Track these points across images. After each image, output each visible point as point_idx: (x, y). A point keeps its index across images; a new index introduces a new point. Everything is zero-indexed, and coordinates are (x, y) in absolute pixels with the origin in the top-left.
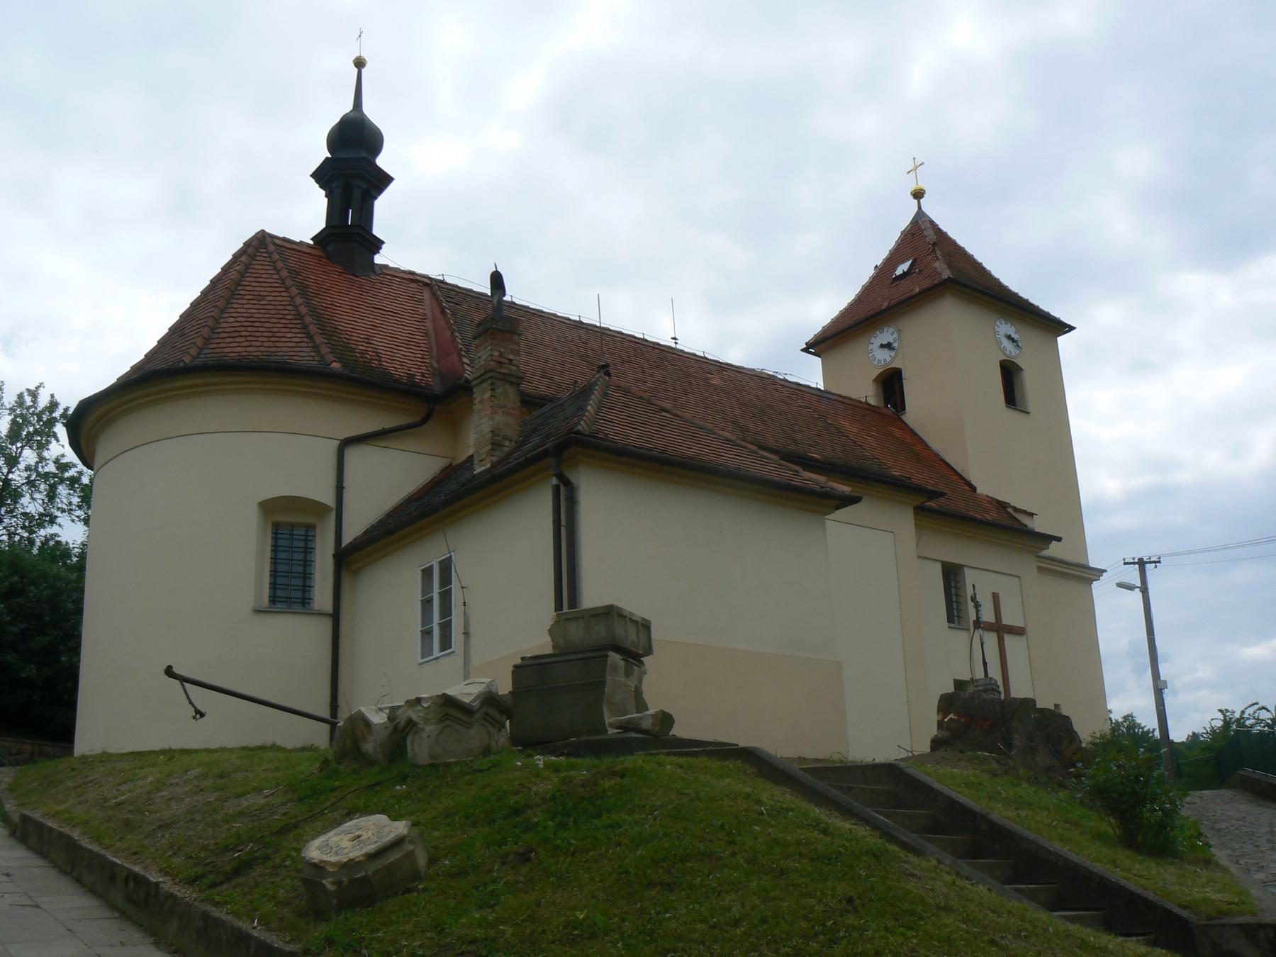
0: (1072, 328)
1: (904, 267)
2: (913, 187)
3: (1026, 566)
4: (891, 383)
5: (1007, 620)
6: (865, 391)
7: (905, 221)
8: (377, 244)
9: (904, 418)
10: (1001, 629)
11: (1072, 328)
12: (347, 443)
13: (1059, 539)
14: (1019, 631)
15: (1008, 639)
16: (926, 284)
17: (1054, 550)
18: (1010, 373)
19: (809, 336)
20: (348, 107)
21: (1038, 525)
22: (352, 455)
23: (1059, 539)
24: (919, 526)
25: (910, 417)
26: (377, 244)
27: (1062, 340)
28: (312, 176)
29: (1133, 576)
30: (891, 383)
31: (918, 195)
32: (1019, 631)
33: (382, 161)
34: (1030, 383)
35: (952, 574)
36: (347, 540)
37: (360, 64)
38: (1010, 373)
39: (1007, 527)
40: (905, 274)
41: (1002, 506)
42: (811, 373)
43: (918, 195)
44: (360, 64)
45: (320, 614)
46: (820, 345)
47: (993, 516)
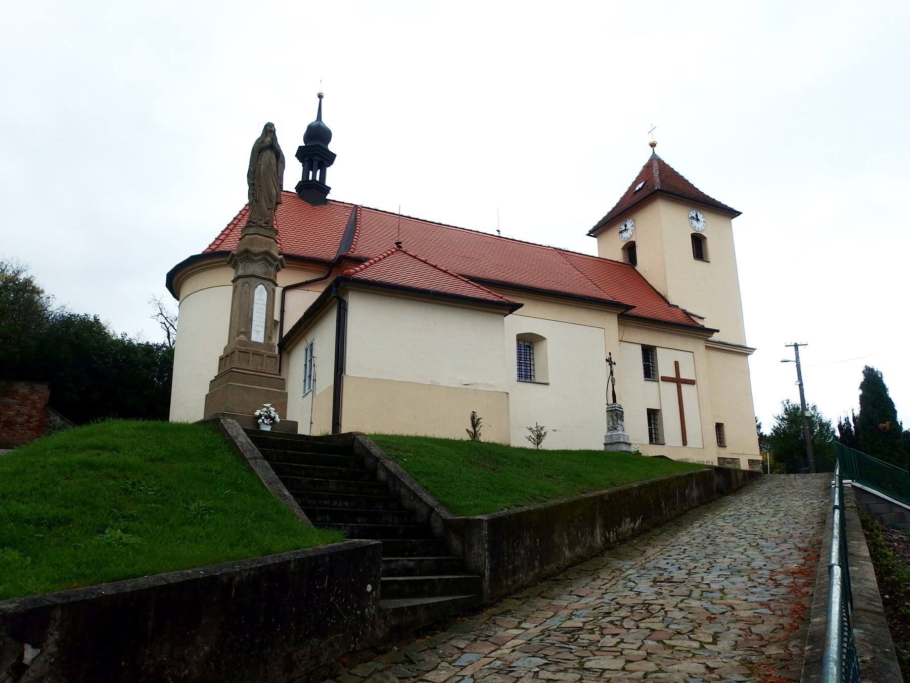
0: (740, 213)
1: (640, 186)
2: (651, 141)
3: (698, 346)
4: (630, 249)
5: (683, 376)
6: (617, 255)
7: (645, 161)
8: (327, 190)
9: (636, 268)
10: (678, 381)
11: (740, 213)
12: (286, 289)
13: (718, 331)
14: (692, 382)
15: (684, 387)
16: (647, 193)
17: (715, 337)
18: (698, 242)
19: (591, 227)
20: (313, 118)
21: (707, 324)
22: (290, 295)
23: (718, 331)
24: (620, 324)
25: (639, 268)
26: (327, 190)
27: (735, 221)
28: (335, 156)
29: (790, 354)
30: (630, 249)
31: (653, 145)
32: (692, 382)
33: (331, 147)
34: (712, 247)
35: (648, 353)
36: (285, 333)
37: (320, 96)
38: (698, 242)
39: (689, 327)
40: (640, 189)
41: (688, 315)
42: (591, 247)
43: (653, 145)
44: (320, 96)
45: (665, 379)
46: (597, 231)
47: (682, 319)
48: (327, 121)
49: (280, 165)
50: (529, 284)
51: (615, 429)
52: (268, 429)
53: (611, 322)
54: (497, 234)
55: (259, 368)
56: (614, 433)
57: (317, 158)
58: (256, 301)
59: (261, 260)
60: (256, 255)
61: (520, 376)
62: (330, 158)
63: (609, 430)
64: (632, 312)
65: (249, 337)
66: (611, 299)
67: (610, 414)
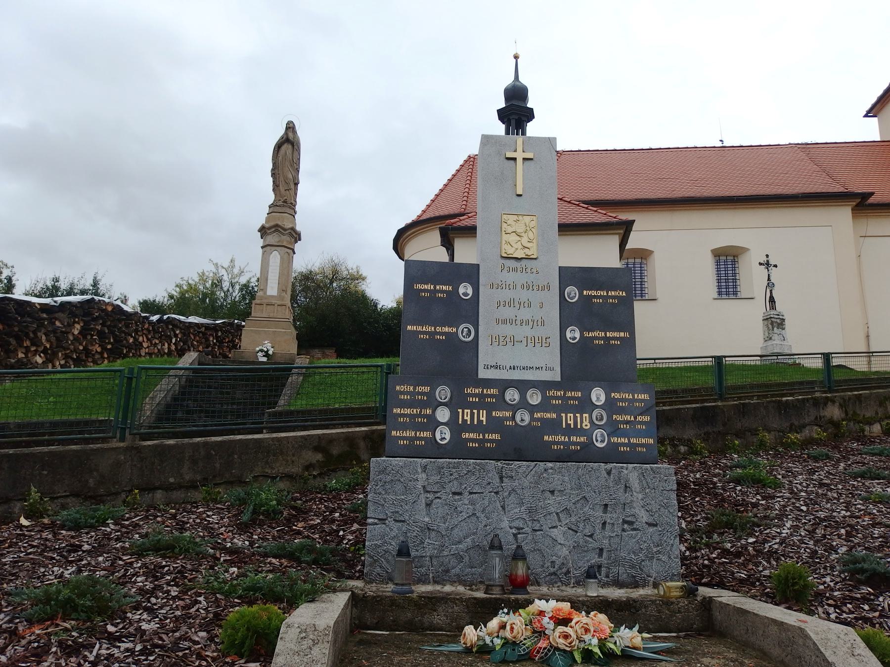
19: (868, 106)
37: (516, 57)
44: (516, 57)
48: (523, 80)
49: (296, 153)
50: (653, 197)
51: (771, 339)
52: (265, 359)
53: (843, 215)
54: (720, 144)
55: (271, 315)
56: (770, 343)
57: (514, 116)
58: (271, 263)
59: (274, 232)
60: (285, 230)
61: (720, 293)
62: (529, 115)
63: (240, 328)
64: (871, 200)
65: (265, 293)
66: (842, 190)
67: (766, 322)
